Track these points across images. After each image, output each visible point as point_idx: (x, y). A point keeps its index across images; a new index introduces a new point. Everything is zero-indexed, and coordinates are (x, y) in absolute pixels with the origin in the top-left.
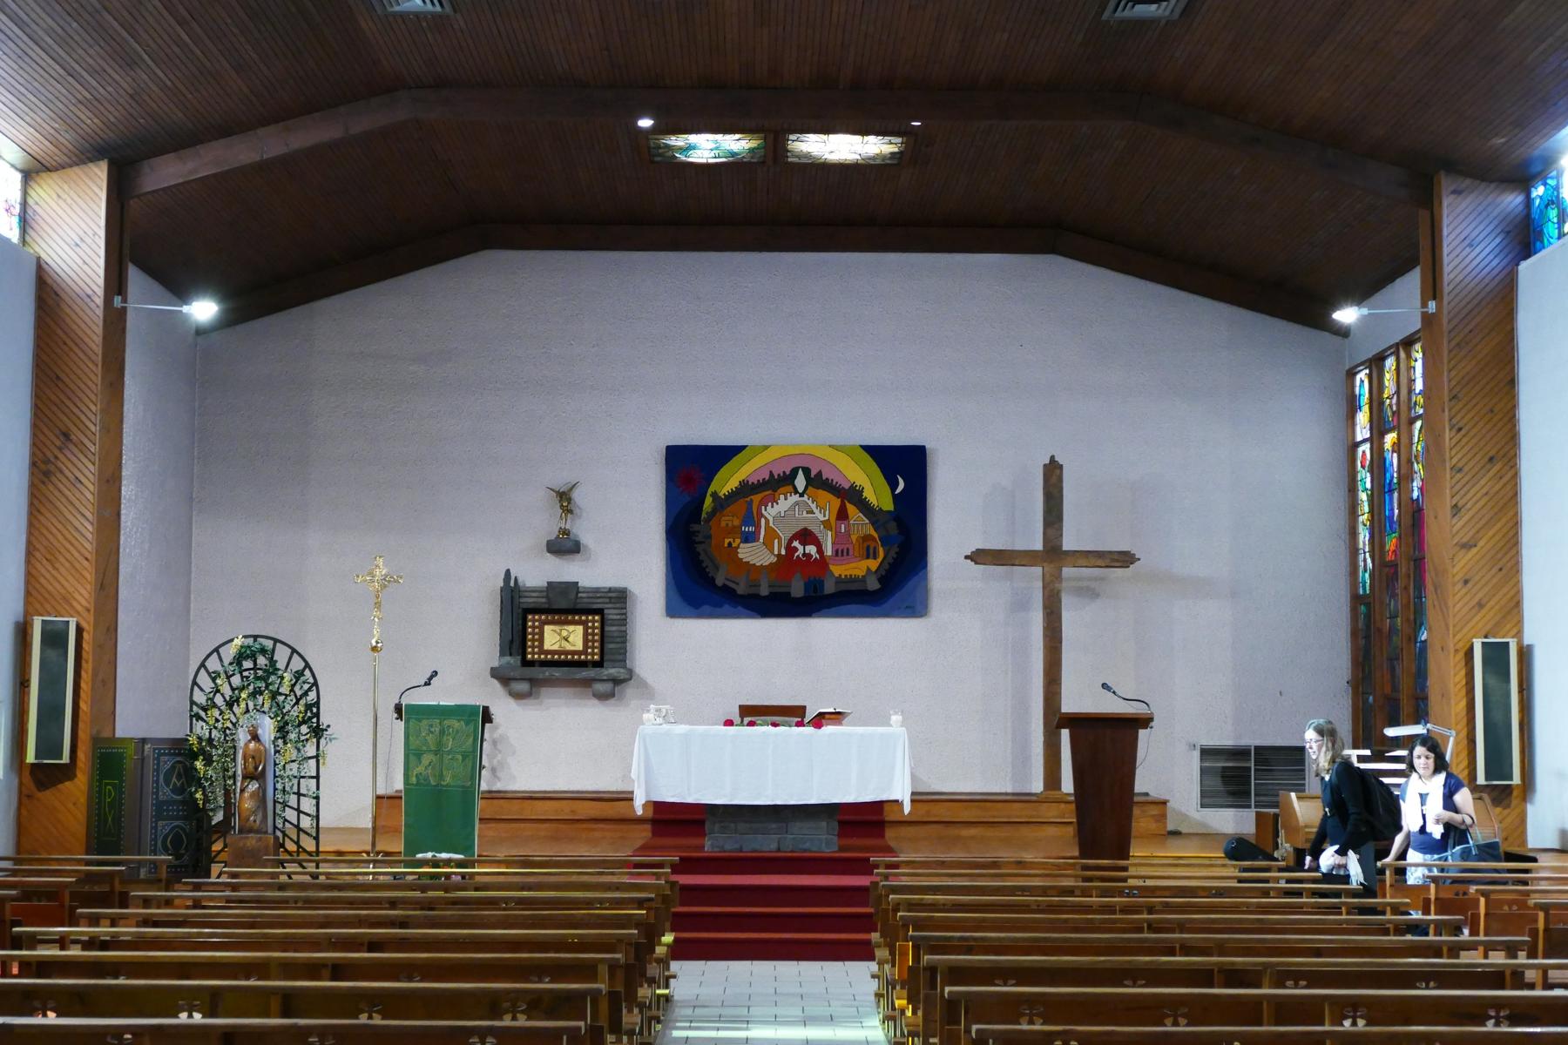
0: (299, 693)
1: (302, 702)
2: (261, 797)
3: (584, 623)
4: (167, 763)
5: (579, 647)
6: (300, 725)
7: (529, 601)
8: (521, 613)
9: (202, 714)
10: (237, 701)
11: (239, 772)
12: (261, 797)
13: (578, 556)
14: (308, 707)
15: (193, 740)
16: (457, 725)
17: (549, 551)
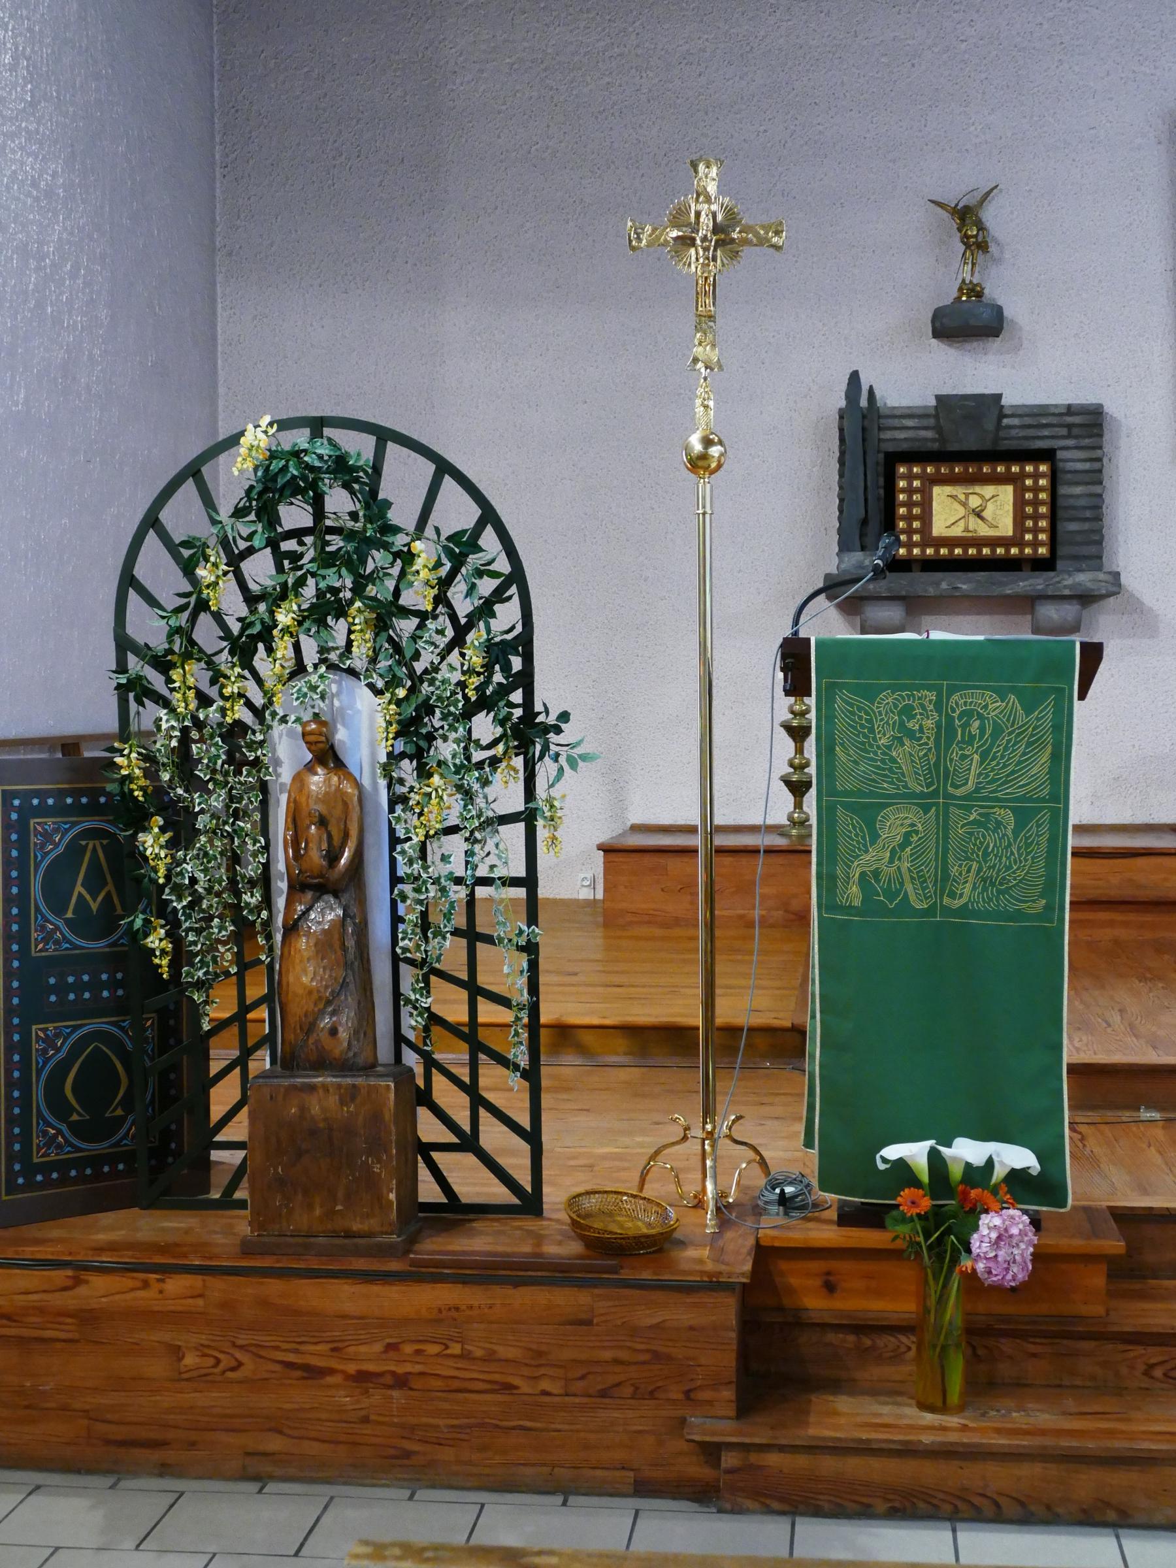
0: (463, 608)
1: (475, 638)
2: (350, 950)
3: (1015, 480)
4: (53, 837)
5: (1006, 527)
6: (468, 714)
7: (898, 437)
8: (881, 461)
9: (156, 680)
10: (266, 636)
12: (350, 950)
13: (995, 344)
14: (496, 652)
15: (129, 763)
16: (994, 706)
17: (938, 333)
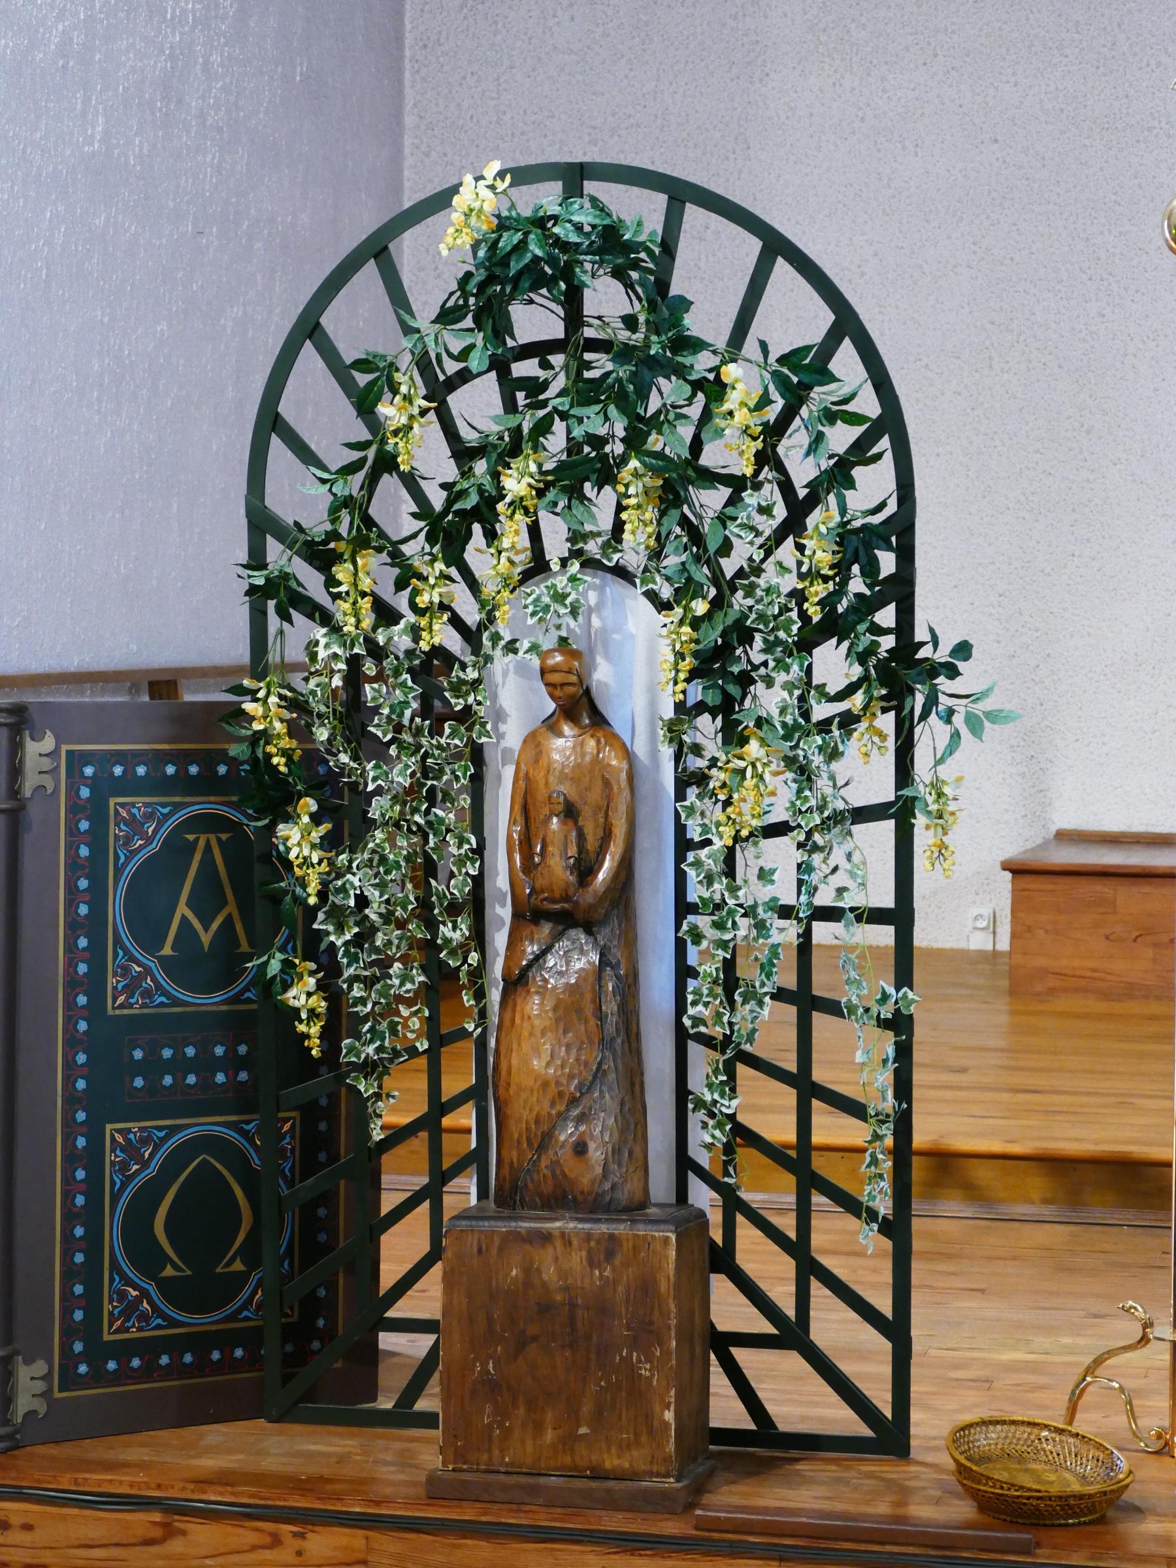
4: (145, 825)
6: (806, 645)
9: (311, 581)
10: (486, 513)
11: (500, 881)
14: (855, 545)
15: (265, 712)
